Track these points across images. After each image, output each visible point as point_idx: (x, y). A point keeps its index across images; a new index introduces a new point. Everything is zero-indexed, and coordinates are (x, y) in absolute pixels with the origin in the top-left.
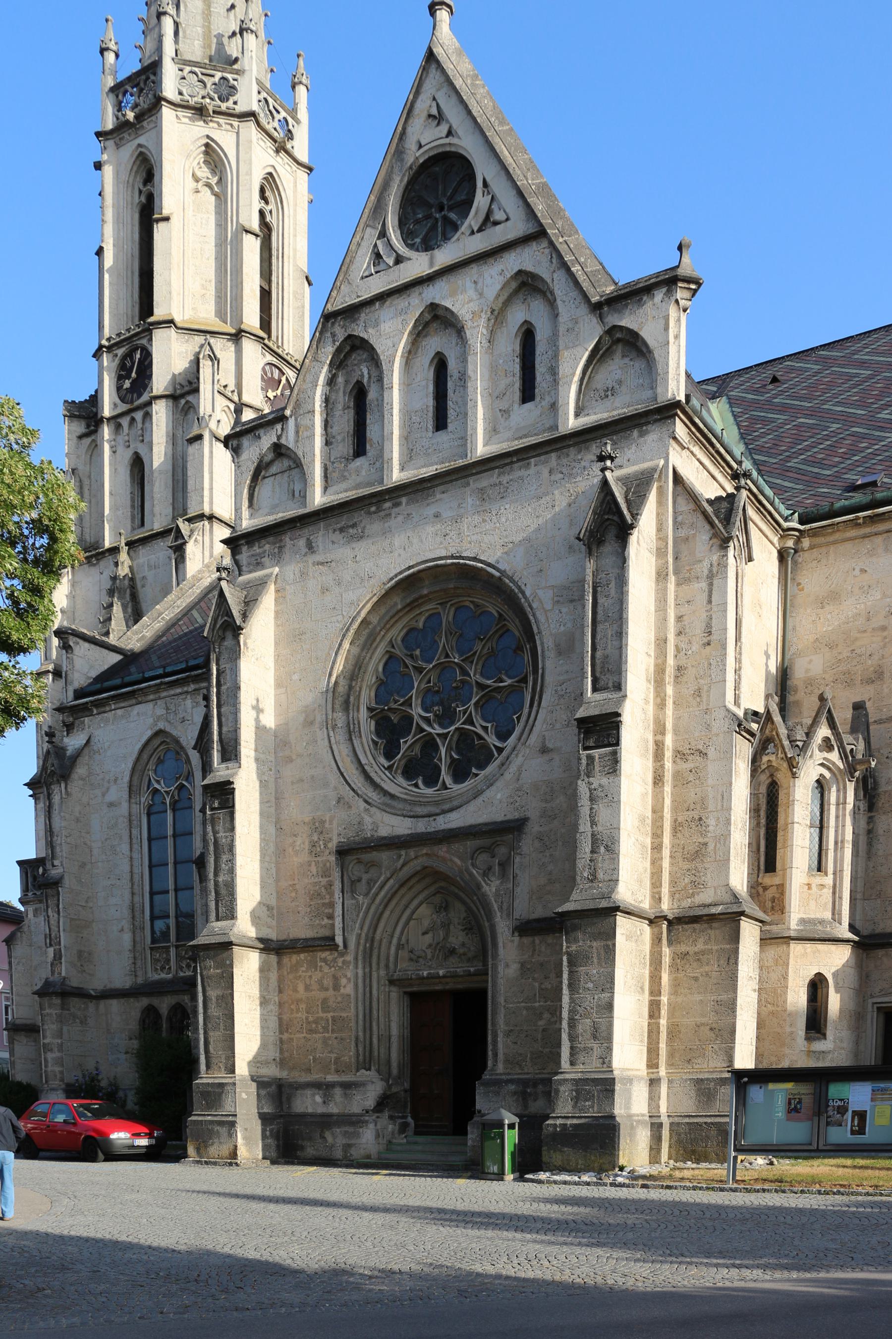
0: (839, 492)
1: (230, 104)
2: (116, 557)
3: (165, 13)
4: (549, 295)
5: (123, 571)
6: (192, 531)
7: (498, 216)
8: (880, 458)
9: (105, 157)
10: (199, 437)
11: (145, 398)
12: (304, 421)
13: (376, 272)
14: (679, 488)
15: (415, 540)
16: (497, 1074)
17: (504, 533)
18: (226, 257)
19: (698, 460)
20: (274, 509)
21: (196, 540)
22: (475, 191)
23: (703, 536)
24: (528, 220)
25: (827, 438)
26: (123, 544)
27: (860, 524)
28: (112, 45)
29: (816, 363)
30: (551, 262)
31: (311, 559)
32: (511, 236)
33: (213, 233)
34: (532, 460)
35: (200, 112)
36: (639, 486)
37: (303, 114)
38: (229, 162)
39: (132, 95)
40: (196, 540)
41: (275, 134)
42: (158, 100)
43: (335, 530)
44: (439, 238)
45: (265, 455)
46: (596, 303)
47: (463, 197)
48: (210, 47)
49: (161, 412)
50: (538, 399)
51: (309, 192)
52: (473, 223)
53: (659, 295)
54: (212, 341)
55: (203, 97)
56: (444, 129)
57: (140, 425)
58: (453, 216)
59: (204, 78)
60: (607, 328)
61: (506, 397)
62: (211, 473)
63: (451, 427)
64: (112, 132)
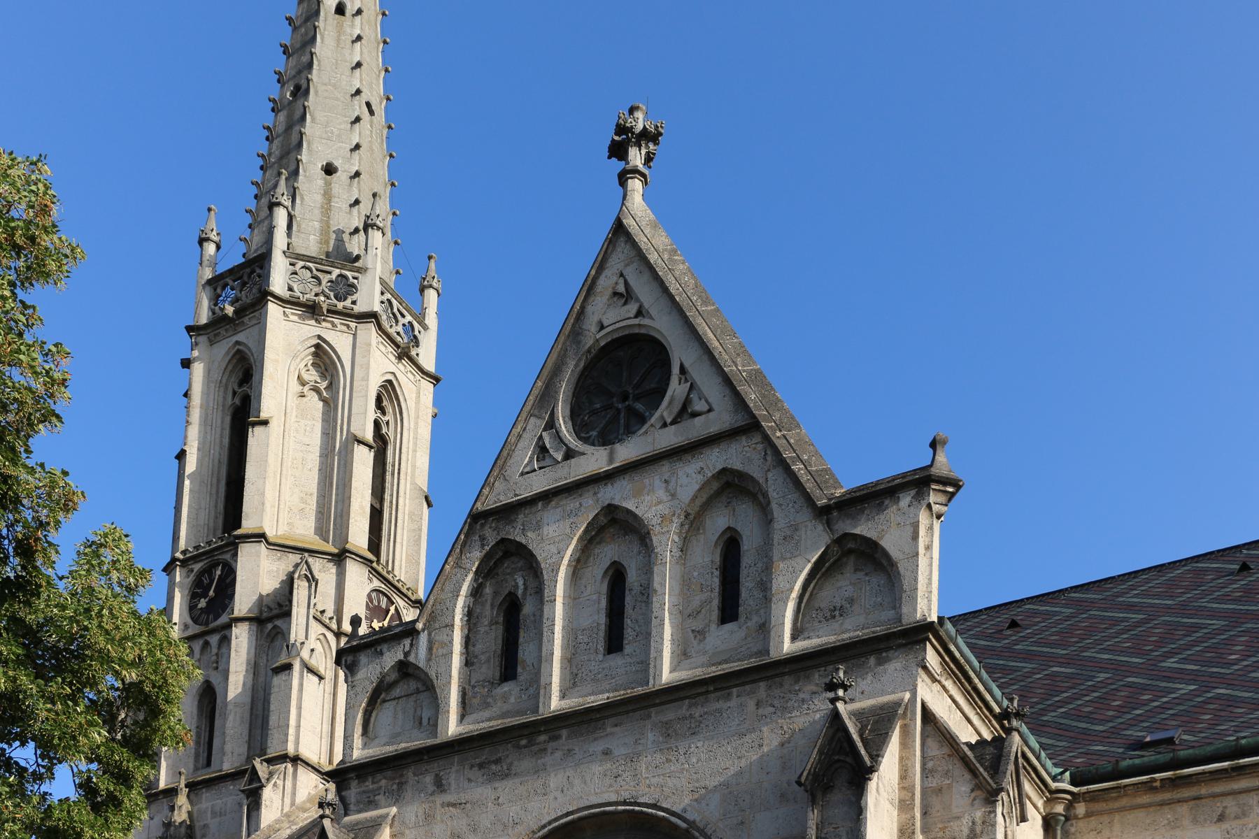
0: (1121, 750)
1: (348, 303)
2: (172, 801)
3: (279, 204)
4: (761, 498)
5: (180, 816)
6: (271, 774)
7: (699, 406)
8: (1171, 712)
9: (196, 353)
10: (288, 667)
11: (224, 619)
12: (440, 637)
13: (540, 468)
14: (929, 728)
15: (577, 782)
17: (695, 777)
18: (333, 469)
19: (951, 697)
20: (394, 738)
21: (275, 785)
22: (669, 379)
23: (961, 789)
24: (736, 411)
25: (1094, 688)
26: (182, 785)
27: (1156, 788)
28: (213, 236)
29: (1066, 606)
30: (765, 459)
31: (440, 799)
32: (714, 429)
33: (319, 442)
34: (735, 690)
35: (312, 310)
36: (880, 723)
37: (432, 319)
38: (342, 366)
39: (232, 289)
40: (275, 785)
41: (399, 339)
42: (264, 295)
43: (472, 767)
44: (621, 431)
45: (387, 674)
46: (822, 507)
47: (653, 386)
48: (327, 242)
49: (241, 637)
50: (742, 619)
51: (434, 405)
52: (665, 414)
53: (905, 499)
54: (310, 560)
55: (316, 295)
56: (632, 308)
57: (215, 651)
58: (639, 406)
59: (319, 274)
60: (836, 536)
61: (701, 616)
62: (299, 708)
63: (628, 649)
64: (206, 326)
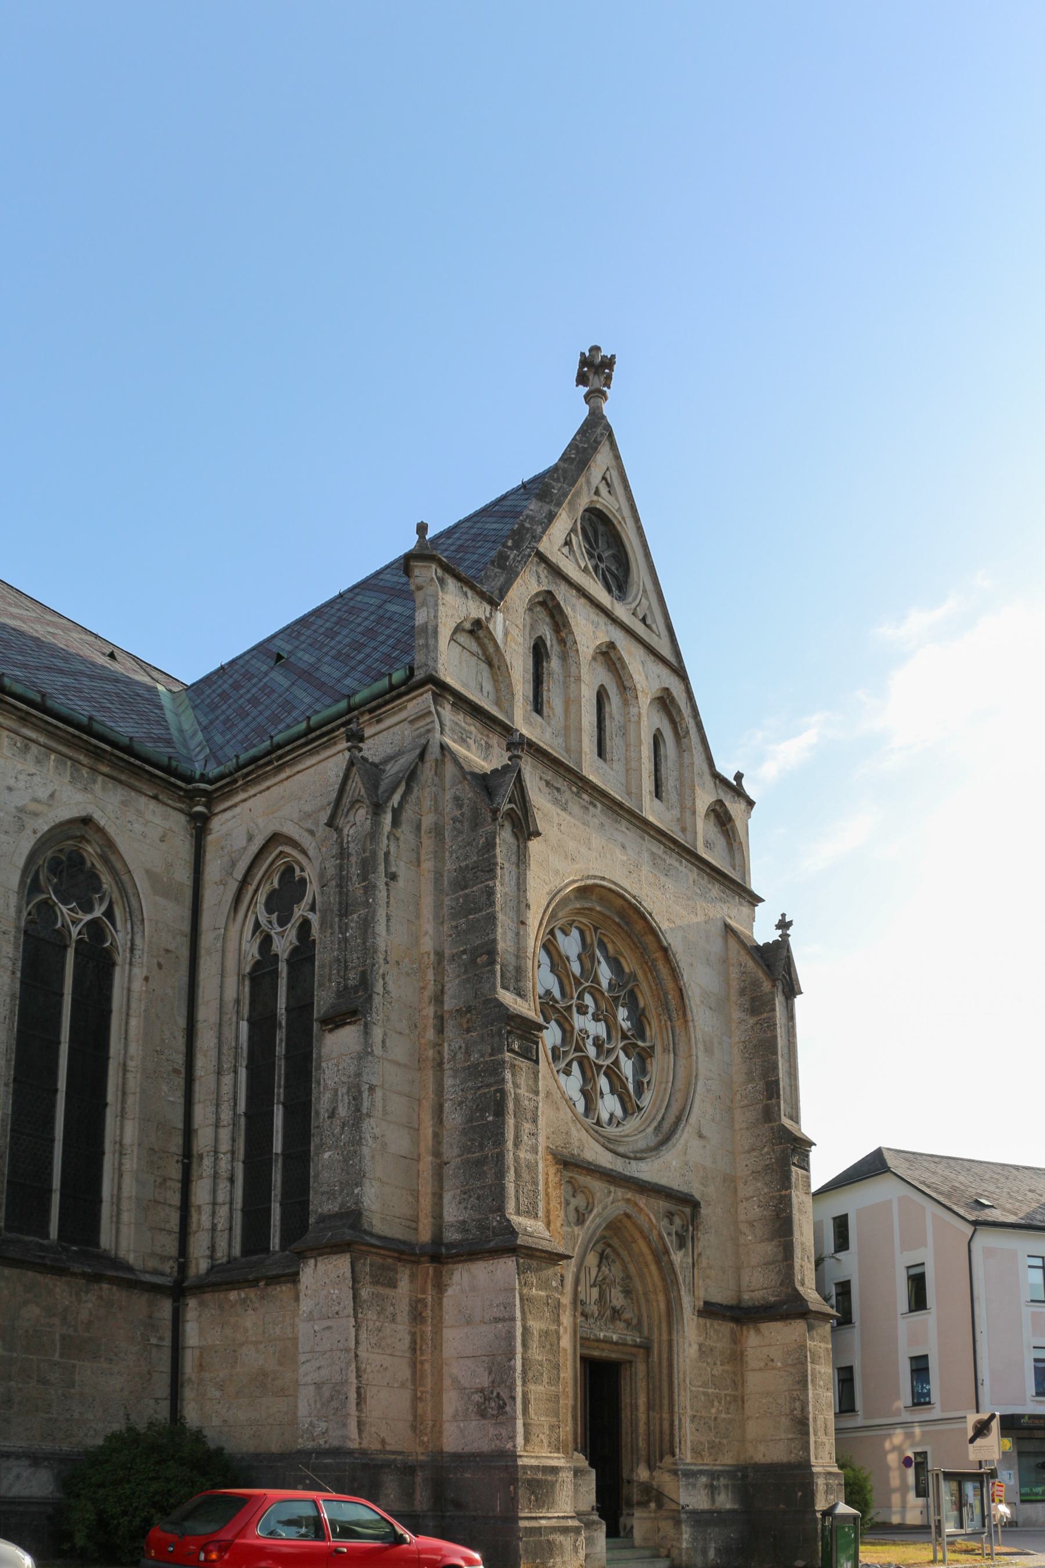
16: (685, 1464)
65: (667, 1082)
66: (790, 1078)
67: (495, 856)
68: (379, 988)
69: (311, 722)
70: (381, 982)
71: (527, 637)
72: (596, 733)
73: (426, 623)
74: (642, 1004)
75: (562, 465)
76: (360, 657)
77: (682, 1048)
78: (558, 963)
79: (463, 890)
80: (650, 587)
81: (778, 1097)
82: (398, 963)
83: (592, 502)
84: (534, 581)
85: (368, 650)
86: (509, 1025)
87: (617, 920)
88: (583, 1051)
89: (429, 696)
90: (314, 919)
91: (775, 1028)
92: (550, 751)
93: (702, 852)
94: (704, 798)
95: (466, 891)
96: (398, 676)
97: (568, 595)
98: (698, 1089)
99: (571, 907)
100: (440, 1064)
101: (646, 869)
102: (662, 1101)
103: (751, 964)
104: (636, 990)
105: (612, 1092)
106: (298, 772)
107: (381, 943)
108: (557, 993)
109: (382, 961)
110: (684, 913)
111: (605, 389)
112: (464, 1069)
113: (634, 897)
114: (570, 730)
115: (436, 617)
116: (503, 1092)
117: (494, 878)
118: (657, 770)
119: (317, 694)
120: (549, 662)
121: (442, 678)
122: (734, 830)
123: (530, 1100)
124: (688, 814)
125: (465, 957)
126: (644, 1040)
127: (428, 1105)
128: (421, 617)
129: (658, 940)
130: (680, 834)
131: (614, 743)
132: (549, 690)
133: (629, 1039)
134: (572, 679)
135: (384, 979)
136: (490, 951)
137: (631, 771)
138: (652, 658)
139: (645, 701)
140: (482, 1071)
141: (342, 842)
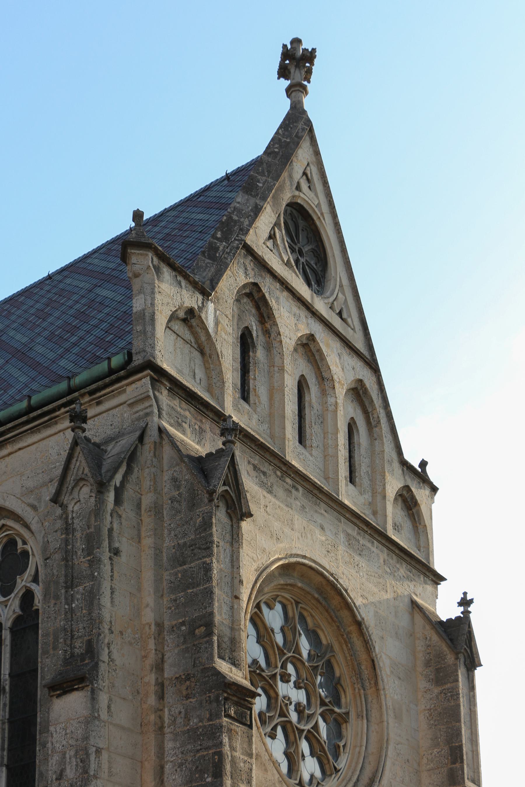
65: (361, 746)
66: (472, 744)
67: (211, 535)
68: (105, 657)
69: (32, 402)
70: (106, 651)
71: (235, 327)
72: (297, 421)
73: (144, 310)
74: (337, 673)
75: (266, 158)
76: (74, 339)
77: (374, 714)
78: (263, 635)
79: (181, 565)
80: (345, 282)
81: (462, 762)
82: (121, 633)
83: (294, 197)
84: (241, 273)
85: (81, 333)
86: (226, 692)
87: (316, 596)
88: (286, 717)
89: (147, 381)
90: (38, 590)
91: (458, 698)
92: (257, 436)
93: (391, 533)
94: (393, 485)
95: (185, 567)
96: (117, 361)
97: (272, 287)
98: (389, 753)
99: (275, 583)
100: (161, 728)
101: (342, 549)
102: (357, 763)
103: (435, 638)
104: (333, 660)
105: (312, 754)
106: (20, 449)
107: (106, 615)
108: (262, 663)
109: (107, 631)
110: (376, 590)
111: (305, 83)
112: (184, 733)
113: (332, 575)
114: (274, 417)
115: (153, 305)
116: (220, 754)
117: (211, 555)
118: (351, 457)
119: (33, 374)
120: (255, 352)
121: (160, 363)
122: (419, 513)
123: (245, 762)
124: (379, 498)
125: (183, 628)
126: (339, 706)
127: (150, 766)
128: (138, 304)
129: (354, 616)
130: (372, 516)
131: (313, 431)
132: (255, 379)
133: (327, 705)
134: (276, 369)
135: (109, 648)
136: (208, 623)
137: (328, 457)
138: (348, 351)
139: (341, 391)
140: (201, 734)
141: (67, 518)
